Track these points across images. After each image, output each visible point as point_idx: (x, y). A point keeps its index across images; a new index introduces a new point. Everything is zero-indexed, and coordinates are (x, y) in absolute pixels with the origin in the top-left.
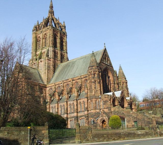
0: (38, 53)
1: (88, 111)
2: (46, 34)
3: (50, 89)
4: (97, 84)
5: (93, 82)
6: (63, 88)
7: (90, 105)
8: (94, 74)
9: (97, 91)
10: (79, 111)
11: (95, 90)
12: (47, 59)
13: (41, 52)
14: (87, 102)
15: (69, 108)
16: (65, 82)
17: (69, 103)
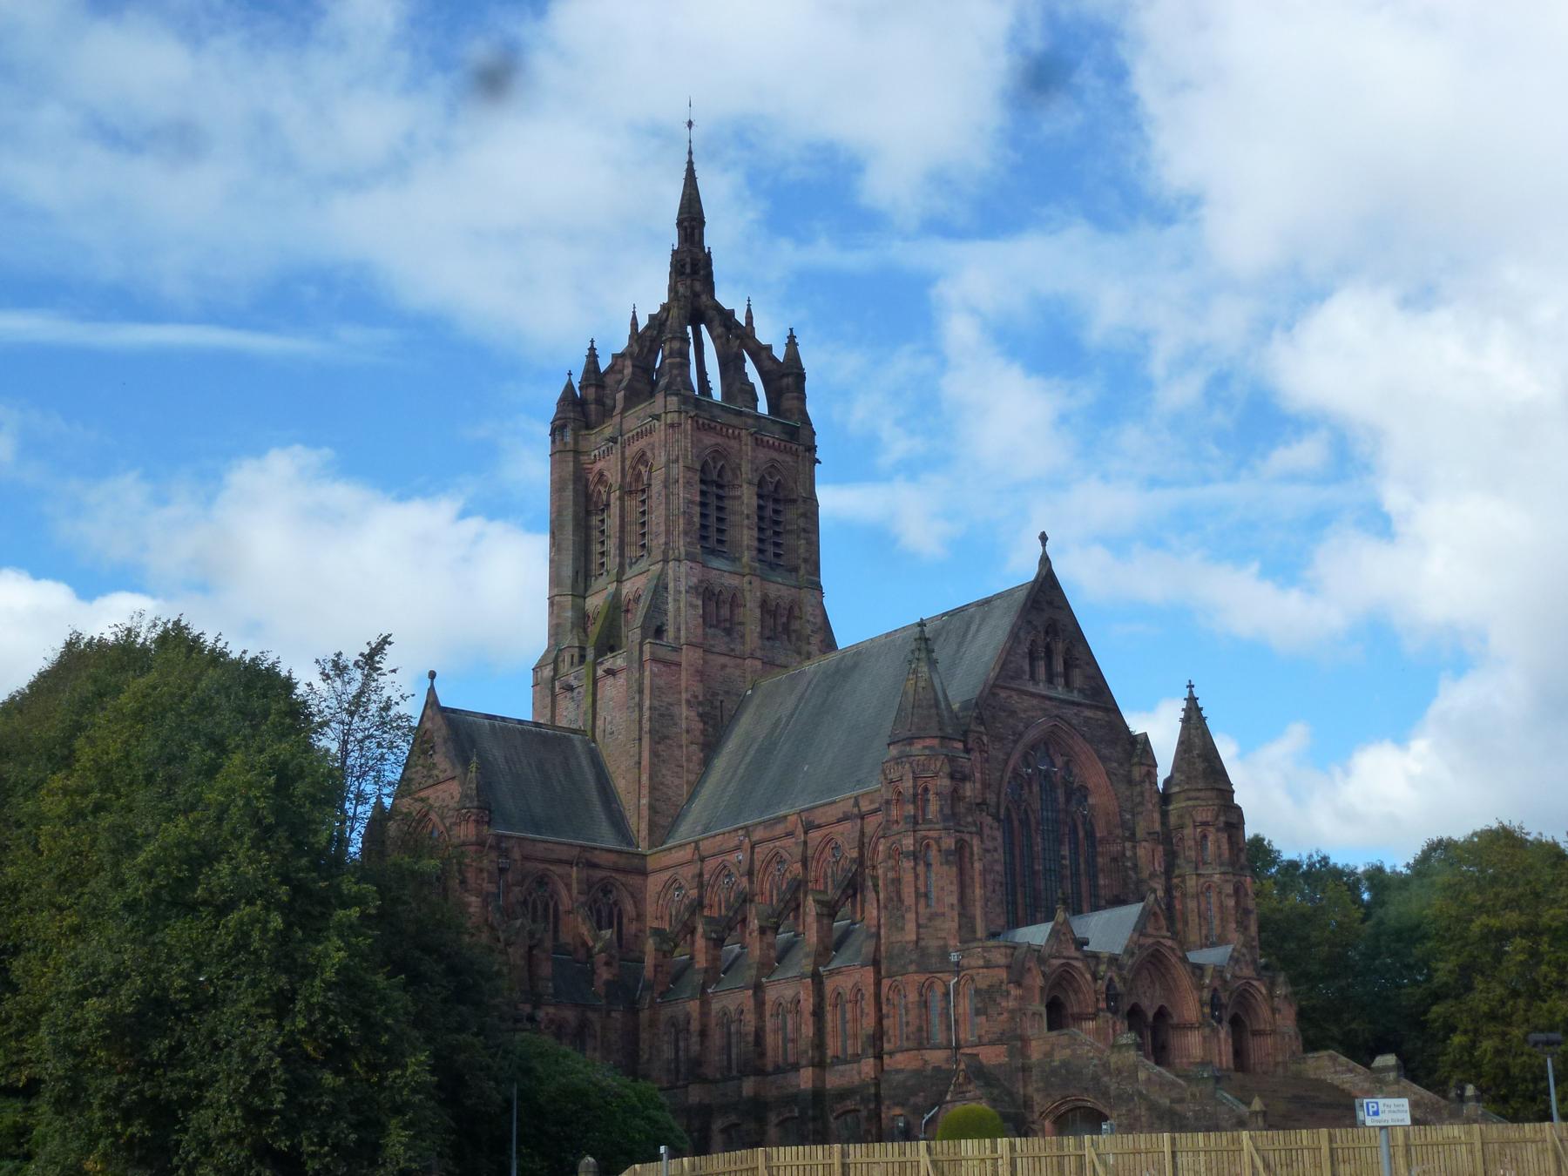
0: (596, 602)
2: (642, 458)
3: (667, 887)
5: (907, 855)
6: (745, 882)
8: (919, 798)
9: (932, 917)
10: (830, 1053)
12: (646, 656)
13: (616, 595)
15: (776, 1032)
16: (758, 835)
17: (771, 995)
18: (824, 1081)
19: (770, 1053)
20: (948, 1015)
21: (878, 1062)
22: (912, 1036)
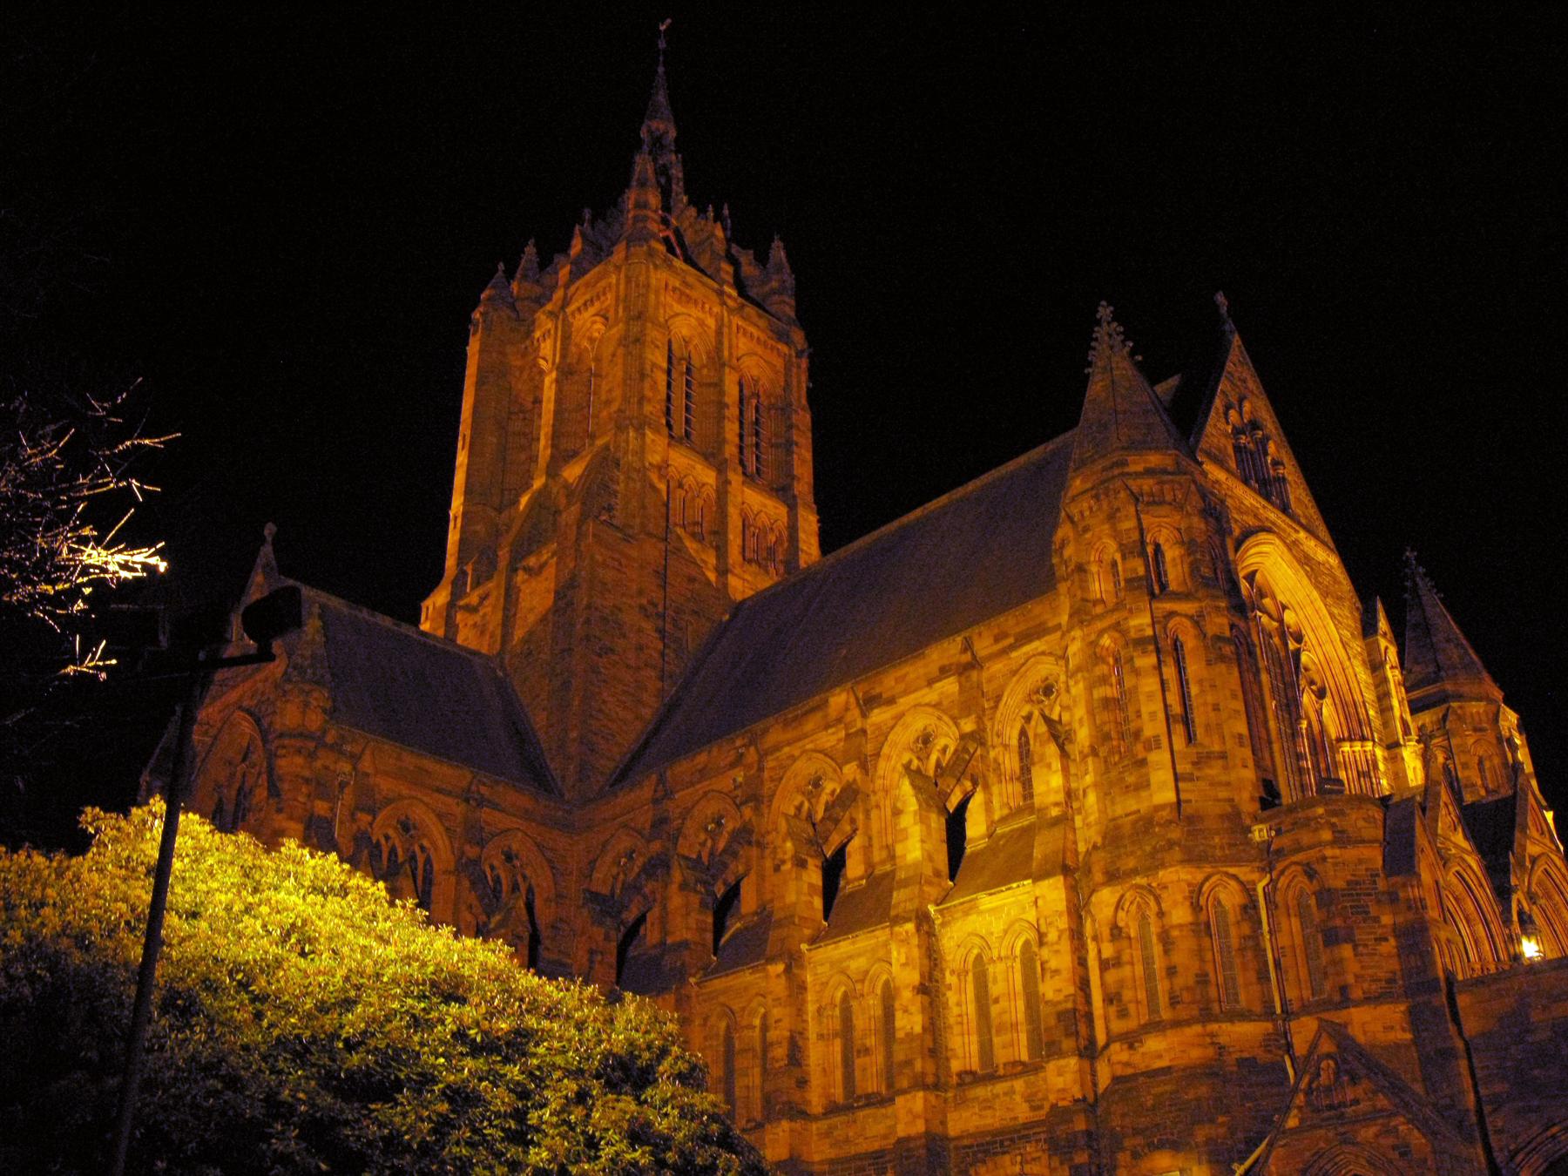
1: (1089, 1052)
4: (1194, 668)
7: (1117, 962)
10: (956, 1066)
11: (1179, 742)
14: (1077, 935)
18: (943, 1123)
19: (816, 1080)
20: (1260, 952)
21: (1086, 1064)
22: (1186, 996)
